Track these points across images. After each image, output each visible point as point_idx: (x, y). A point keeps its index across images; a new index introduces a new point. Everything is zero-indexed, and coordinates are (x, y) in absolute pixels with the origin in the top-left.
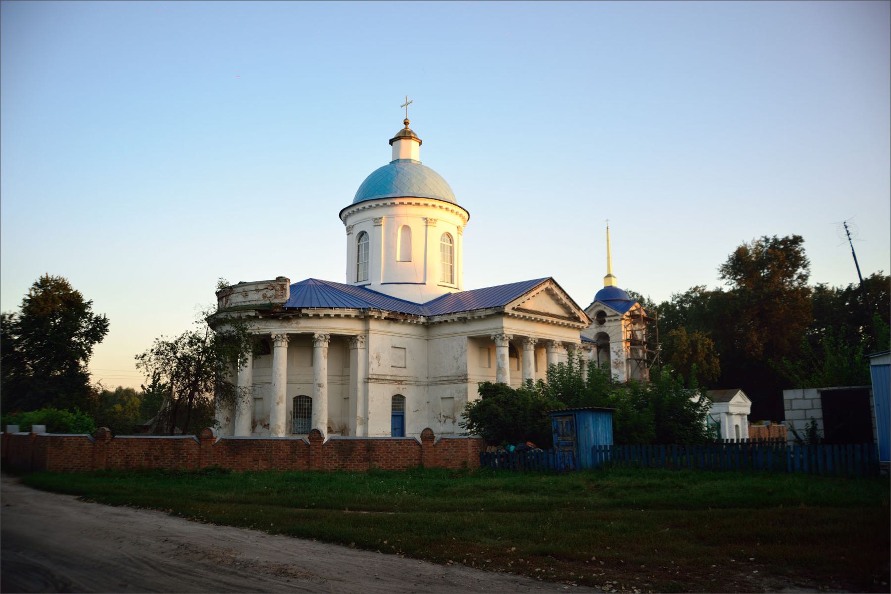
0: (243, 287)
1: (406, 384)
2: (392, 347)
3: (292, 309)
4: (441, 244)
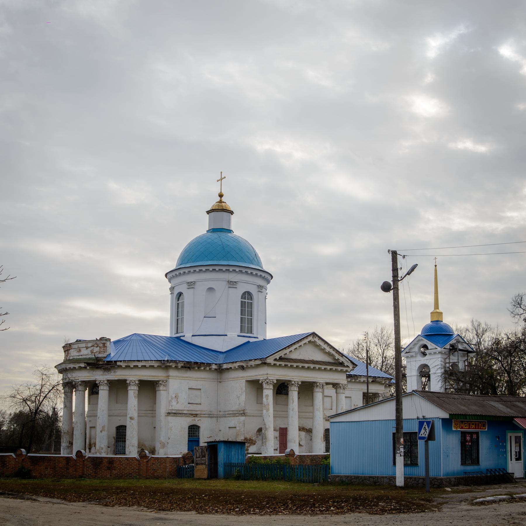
0: (78, 345)
1: (201, 417)
2: (189, 388)
3: (109, 362)
4: (242, 301)
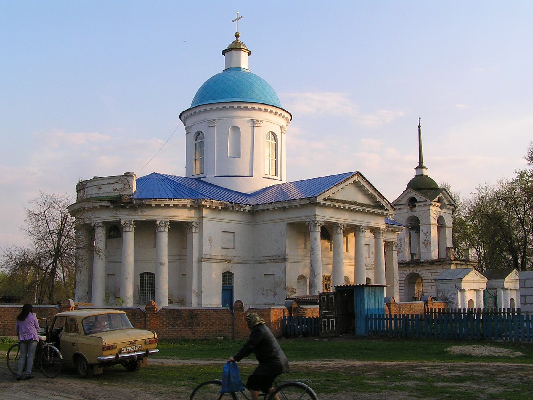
0: (98, 182)
2: (222, 231)
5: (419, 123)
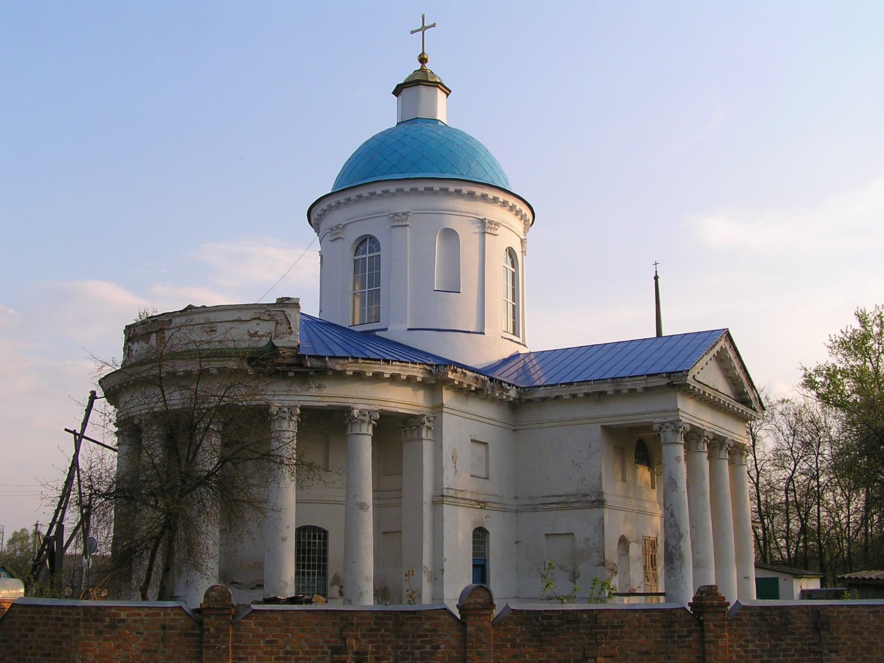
5: (656, 272)
